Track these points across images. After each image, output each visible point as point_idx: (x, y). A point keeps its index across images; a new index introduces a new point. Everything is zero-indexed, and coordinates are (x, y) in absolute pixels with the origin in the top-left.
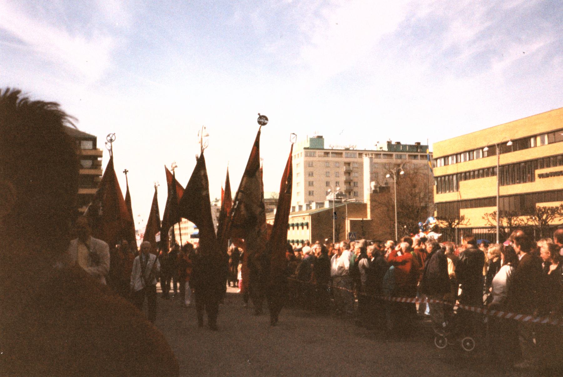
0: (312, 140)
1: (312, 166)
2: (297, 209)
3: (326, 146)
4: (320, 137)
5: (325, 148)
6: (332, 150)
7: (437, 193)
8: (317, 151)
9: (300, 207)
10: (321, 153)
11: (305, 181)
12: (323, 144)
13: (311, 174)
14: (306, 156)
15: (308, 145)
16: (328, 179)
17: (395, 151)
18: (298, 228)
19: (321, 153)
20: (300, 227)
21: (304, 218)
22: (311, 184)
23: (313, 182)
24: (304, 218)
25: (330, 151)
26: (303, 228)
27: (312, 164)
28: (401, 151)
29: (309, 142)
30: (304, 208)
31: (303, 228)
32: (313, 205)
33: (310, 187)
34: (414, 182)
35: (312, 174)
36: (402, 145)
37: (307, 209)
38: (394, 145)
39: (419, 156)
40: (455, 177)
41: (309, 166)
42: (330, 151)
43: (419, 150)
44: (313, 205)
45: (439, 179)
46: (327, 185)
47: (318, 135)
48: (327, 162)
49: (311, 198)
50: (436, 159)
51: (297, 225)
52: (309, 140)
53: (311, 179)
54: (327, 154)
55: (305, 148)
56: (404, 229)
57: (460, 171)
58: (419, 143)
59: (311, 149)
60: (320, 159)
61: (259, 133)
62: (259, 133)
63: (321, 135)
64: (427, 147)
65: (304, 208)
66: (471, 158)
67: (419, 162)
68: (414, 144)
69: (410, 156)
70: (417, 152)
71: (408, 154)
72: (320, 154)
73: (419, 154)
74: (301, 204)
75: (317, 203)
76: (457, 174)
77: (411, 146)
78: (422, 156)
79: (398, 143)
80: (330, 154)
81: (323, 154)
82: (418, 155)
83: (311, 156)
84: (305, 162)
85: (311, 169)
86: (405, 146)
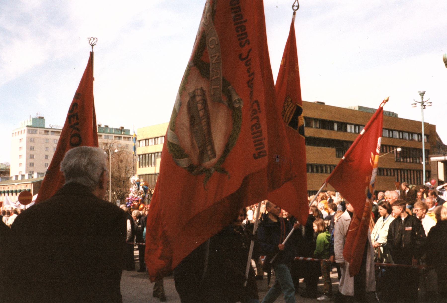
0: (34, 120)
1: (34, 141)
2: (14, 179)
3: (47, 126)
4: (42, 118)
5: (46, 126)
6: (51, 129)
7: (139, 167)
8: (38, 129)
9: (23, 176)
10: (42, 131)
11: (27, 153)
12: (44, 124)
13: (32, 149)
14: (29, 132)
15: (30, 124)
16: (47, 153)
17: (104, 133)
18: (5, 195)
19: (42, 131)
20: (10, 194)
21: (12, 187)
22: (32, 157)
23: (33, 156)
24: (27, 186)
25: (50, 130)
26: (12, 195)
27: (34, 140)
28: (109, 133)
29: (31, 122)
30: (26, 177)
31: (12, 195)
32: (35, 175)
33: (31, 159)
34: (121, 158)
35: (33, 148)
36: (110, 128)
37: (29, 178)
38: (103, 128)
39: (123, 138)
40: (153, 155)
41: (31, 142)
42: (50, 130)
43: (122, 133)
44: (35, 175)
45: (141, 156)
46: (46, 158)
47: (39, 116)
48: (47, 139)
49: (31, 169)
50: (139, 141)
51: (8, 192)
52: (31, 119)
53: (32, 153)
54: (47, 132)
55: (28, 126)
56: (114, 195)
57: (157, 151)
58: (122, 128)
59: (33, 127)
60: (41, 136)
61: (92, 54)
62: (92, 54)
63: (42, 116)
64: (129, 131)
65: (26, 177)
66: (157, 143)
67: (123, 142)
68: (119, 128)
69: (115, 137)
70: (121, 134)
71: (114, 135)
72: (41, 132)
73: (123, 136)
74: (23, 174)
75: (38, 173)
76: (155, 153)
77: (116, 129)
78: (125, 138)
79: (107, 126)
80: (50, 133)
81: (43, 132)
82: (121, 137)
83: (32, 133)
84: (28, 138)
85: (32, 144)
86: (112, 129)
